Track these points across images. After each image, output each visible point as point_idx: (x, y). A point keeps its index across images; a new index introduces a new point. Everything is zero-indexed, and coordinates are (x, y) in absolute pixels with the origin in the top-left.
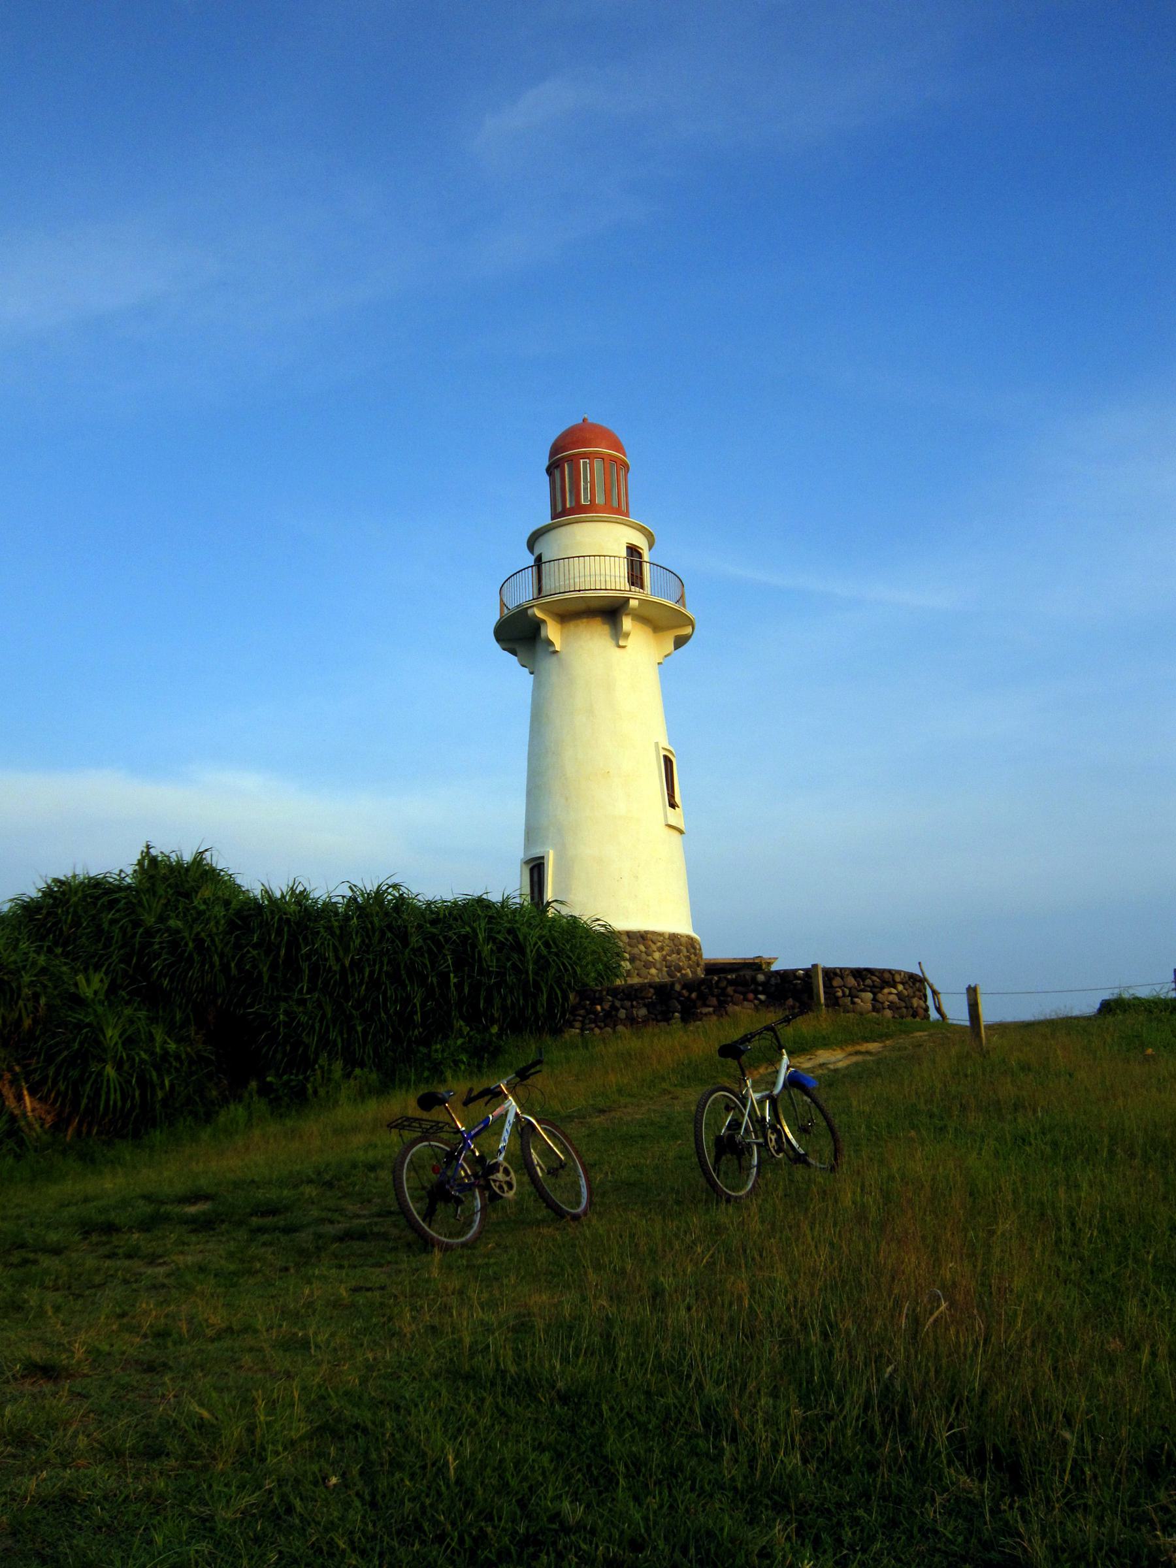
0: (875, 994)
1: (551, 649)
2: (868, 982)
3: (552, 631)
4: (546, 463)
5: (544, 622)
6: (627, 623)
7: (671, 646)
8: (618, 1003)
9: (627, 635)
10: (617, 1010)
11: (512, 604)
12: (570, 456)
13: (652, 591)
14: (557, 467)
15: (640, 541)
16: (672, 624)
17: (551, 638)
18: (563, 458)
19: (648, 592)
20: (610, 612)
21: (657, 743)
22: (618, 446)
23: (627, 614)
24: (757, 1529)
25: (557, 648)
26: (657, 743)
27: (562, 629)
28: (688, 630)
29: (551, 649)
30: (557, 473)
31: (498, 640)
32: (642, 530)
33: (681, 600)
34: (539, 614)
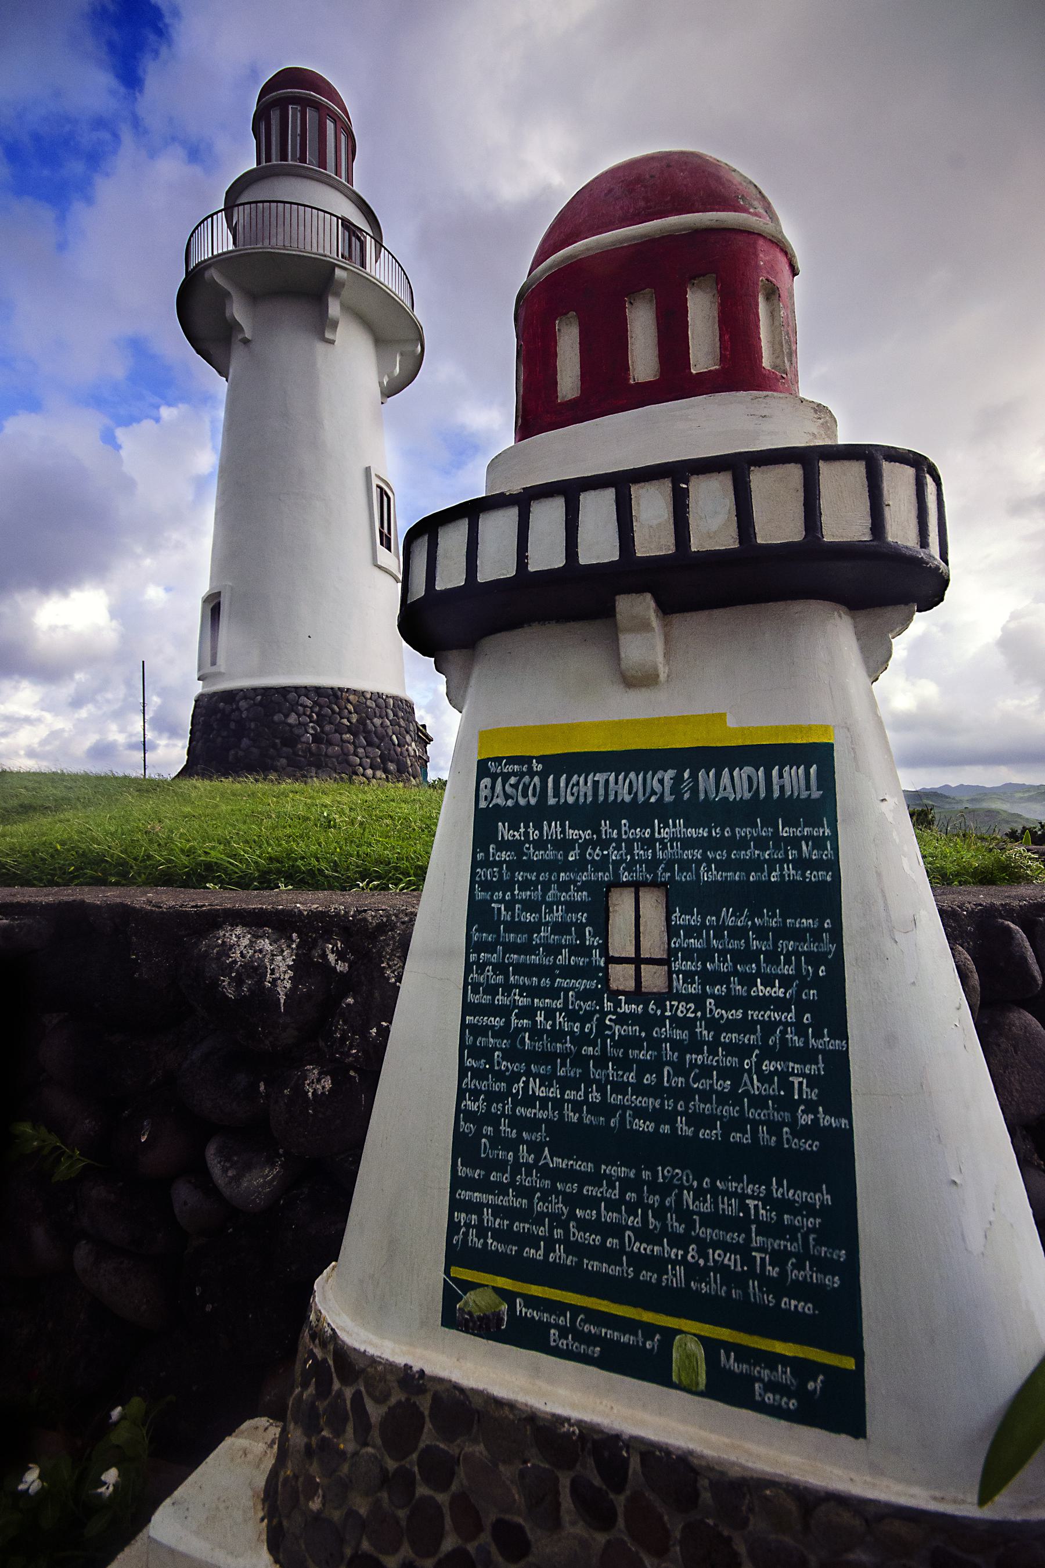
1: (240, 337)
5: (228, 294)
21: (368, 470)
24: (292, 719)
25: (248, 335)
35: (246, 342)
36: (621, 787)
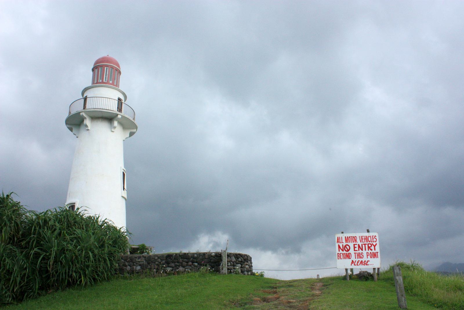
0: (242, 265)
1: (87, 129)
2: (240, 259)
3: (87, 122)
4: (92, 67)
5: (85, 118)
6: (116, 123)
7: (128, 135)
8: (127, 264)
9: (115, 128)
10: (126, 266)
11: (73, 112)
12: (101, 65)
13: (126, 112)
14: (96, 68)
15: (122, 97)
16: (129, 126)
17: (87, 124)
18: (99, 65)
19: (123, 114)
20: (109, 118)
22: (119, 67)
23: (116, 120)
25: (89, 128)
26: (121, 167)
27: (92, 121)
28: (135, 130)
29: (87, 129)
30: (96, 71)
31: (66, 124)
32: (124, 94)
33: (134, 119)
34: (85, 115)
35: (88, 130)
36: (115, 81)
